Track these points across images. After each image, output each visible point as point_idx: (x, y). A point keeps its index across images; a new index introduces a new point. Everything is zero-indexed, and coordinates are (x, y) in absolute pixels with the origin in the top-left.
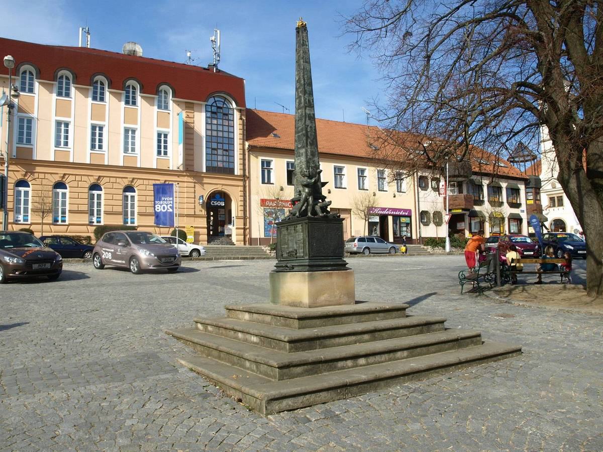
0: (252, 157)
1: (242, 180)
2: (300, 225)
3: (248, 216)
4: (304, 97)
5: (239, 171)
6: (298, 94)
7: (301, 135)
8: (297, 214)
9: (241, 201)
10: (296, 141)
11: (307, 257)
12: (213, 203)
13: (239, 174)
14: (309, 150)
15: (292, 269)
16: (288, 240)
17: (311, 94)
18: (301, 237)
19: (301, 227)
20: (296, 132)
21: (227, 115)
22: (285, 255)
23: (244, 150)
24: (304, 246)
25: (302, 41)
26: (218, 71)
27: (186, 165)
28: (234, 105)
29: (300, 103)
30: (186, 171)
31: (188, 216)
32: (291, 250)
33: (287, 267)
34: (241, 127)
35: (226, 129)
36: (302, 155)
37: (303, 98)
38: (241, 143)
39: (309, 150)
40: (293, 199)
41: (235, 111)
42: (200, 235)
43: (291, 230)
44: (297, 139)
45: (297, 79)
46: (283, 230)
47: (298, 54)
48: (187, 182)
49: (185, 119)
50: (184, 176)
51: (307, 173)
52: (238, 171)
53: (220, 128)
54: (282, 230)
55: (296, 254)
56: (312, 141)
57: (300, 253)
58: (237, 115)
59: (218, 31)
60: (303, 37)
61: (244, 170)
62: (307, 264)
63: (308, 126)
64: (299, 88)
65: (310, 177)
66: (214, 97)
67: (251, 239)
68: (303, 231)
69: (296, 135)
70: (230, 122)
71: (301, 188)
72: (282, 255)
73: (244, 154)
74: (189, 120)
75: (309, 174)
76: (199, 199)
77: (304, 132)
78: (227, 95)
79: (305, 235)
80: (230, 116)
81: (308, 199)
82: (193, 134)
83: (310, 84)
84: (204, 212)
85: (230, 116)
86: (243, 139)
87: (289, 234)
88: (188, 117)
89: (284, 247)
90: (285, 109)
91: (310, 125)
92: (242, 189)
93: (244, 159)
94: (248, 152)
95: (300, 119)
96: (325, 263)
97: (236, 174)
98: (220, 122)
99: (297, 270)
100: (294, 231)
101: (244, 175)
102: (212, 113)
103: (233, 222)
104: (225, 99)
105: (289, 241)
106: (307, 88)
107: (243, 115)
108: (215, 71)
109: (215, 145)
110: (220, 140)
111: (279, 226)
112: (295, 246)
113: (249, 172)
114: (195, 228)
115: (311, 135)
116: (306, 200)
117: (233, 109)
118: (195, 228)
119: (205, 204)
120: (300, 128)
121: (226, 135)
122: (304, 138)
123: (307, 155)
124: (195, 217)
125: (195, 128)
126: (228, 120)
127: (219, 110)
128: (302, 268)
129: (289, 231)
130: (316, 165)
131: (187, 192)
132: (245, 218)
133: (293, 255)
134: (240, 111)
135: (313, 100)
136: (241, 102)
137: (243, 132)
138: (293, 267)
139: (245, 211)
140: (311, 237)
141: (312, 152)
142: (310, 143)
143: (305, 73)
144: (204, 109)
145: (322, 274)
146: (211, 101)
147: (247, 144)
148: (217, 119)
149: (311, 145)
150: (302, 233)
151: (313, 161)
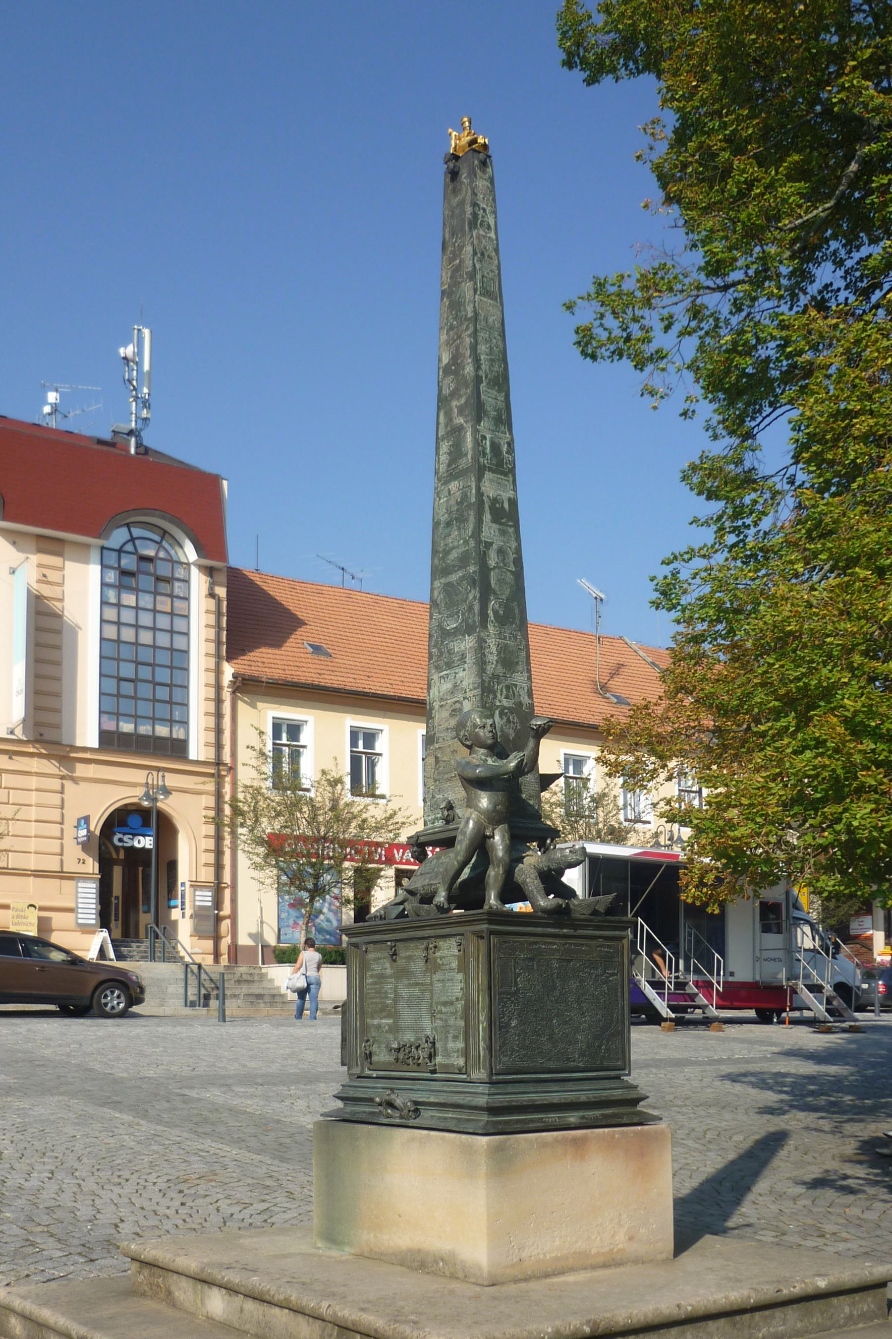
0: (241, 706)
1: (212, 775)
2: (453, 942)
3: (581, 932)
4: (475, 431)
5: (202, 747)
6: (450, 420)
7: (462, 579)
8: (441, 897)
9: (207, 851)
10: (434, 603)
11: (481, 1074)
12: (120, 840)
13: (202, 758)
14: (492, 644)
15: (411, 1117)
16: (396, 1000)
17: (504, 420)
18: (456, 989)
19: (456, 952)
20: (437, 572)
21: (169, 580)
22: (382, 1056)
23: (218, 687)
24: (467, 1026)
25: (469, 210)
26: (142, 450)
27: (37, 724)
28: (190, 552)
29: (456, 453)
30: (36, 741)
31: (38, 874)
32: (408, 1037)
33: (390, 1105)
34: (212, 634)
35: (163, 622)
36: (463, 657)
37: (469, 434)
38: (212, 666)
39: (492, 644)
40: (418, 835)
41: (194, 571)
42: (52, 931)
43: (409, 958)
44: (439, 597)
45: (445, 360)
46: (377, 959)
47: (451, 261)
48: (37, 774)
49: (35, 585)
50: (31, 755)
51: (484, 734)
52: (199, 748)
53: (146, 619)
54: (371, 956)
55: (431, 1056)
56: (507, 607)
57: (451, 1052)
58: (198, 582)
59: (146, 332)
60: (474, 194)
61: (219, 746)
62: (482, 1101)
63: (488, 545)
64: (454, 394)
65: (498, 750)
66: (128, 525)
67: (234, 949)
68: (463, 967)
69: (437, 584)
70: (178, 603)
71: (456, 793)
72: (370, 1055)
73: (219, 701)
74: (46, 591)
75: (494, 737)
76: (77, 827)
77: (472, 569)
78: (171, 522)
79: (473, 986)
80: (177, 584)
81: (485, 838)
82: (59, 632)
83: (501, 382)
84: (92, 866)
85: (177, 584)
86: (218, 656)
87: (402, 974)
88: (44, 580)
89: (379, 1027)
90: (347, 577)
91: (498, 543)
92: (211, 801)
93: (219, 715)
94: (234, 692)
95: (457, 519)
96: (555, 1097)
97: (192, 756)
98: (146, 600)
99: (433, 1124)
100: (421, 963)
101: (218, 763)
102: (124, 573)
103: (183, 897)
104: (164, 533)
105: (402, 1005)
106: (490, 398)
107: (220, 585)
108: (133, 451)
109: (127, 670)
110: (146, 655)
111: (354, 940)
112: (427, 1023)
113: (234, 754)
114: (41, 909)
115: (500, 581)
116: (481, 845)
117: (188, 564)
118: (41, 909)
119: (96, 843)
120: (454, 554)
121: (163, 640)
122: (474, 594)
123: (481, 663)
124: (62, 878)
125: (66, 613)
126: (172, 596)
127: (144, 565)
128: (455, 1119)
129: (401, 962)
130: (520, 704)
131: (38, 805)
132: (218, 889)
133: (416, 1060)
134: (210, 571)
135: (510, 444)
136: (211, 545)
137: (218, 635)
138: (417, 1108)
139: (219, 867)
140: (499, 989)
141: (503, 649)
142: (496, 613)
143: (482, 335)
144: (95, 555)
145: (545, 1145)
146: (119, 537)
147: (228, 671)
148: (136, 590)
149: (502, 621)
150: (460, 976)
151: (508, 687)
